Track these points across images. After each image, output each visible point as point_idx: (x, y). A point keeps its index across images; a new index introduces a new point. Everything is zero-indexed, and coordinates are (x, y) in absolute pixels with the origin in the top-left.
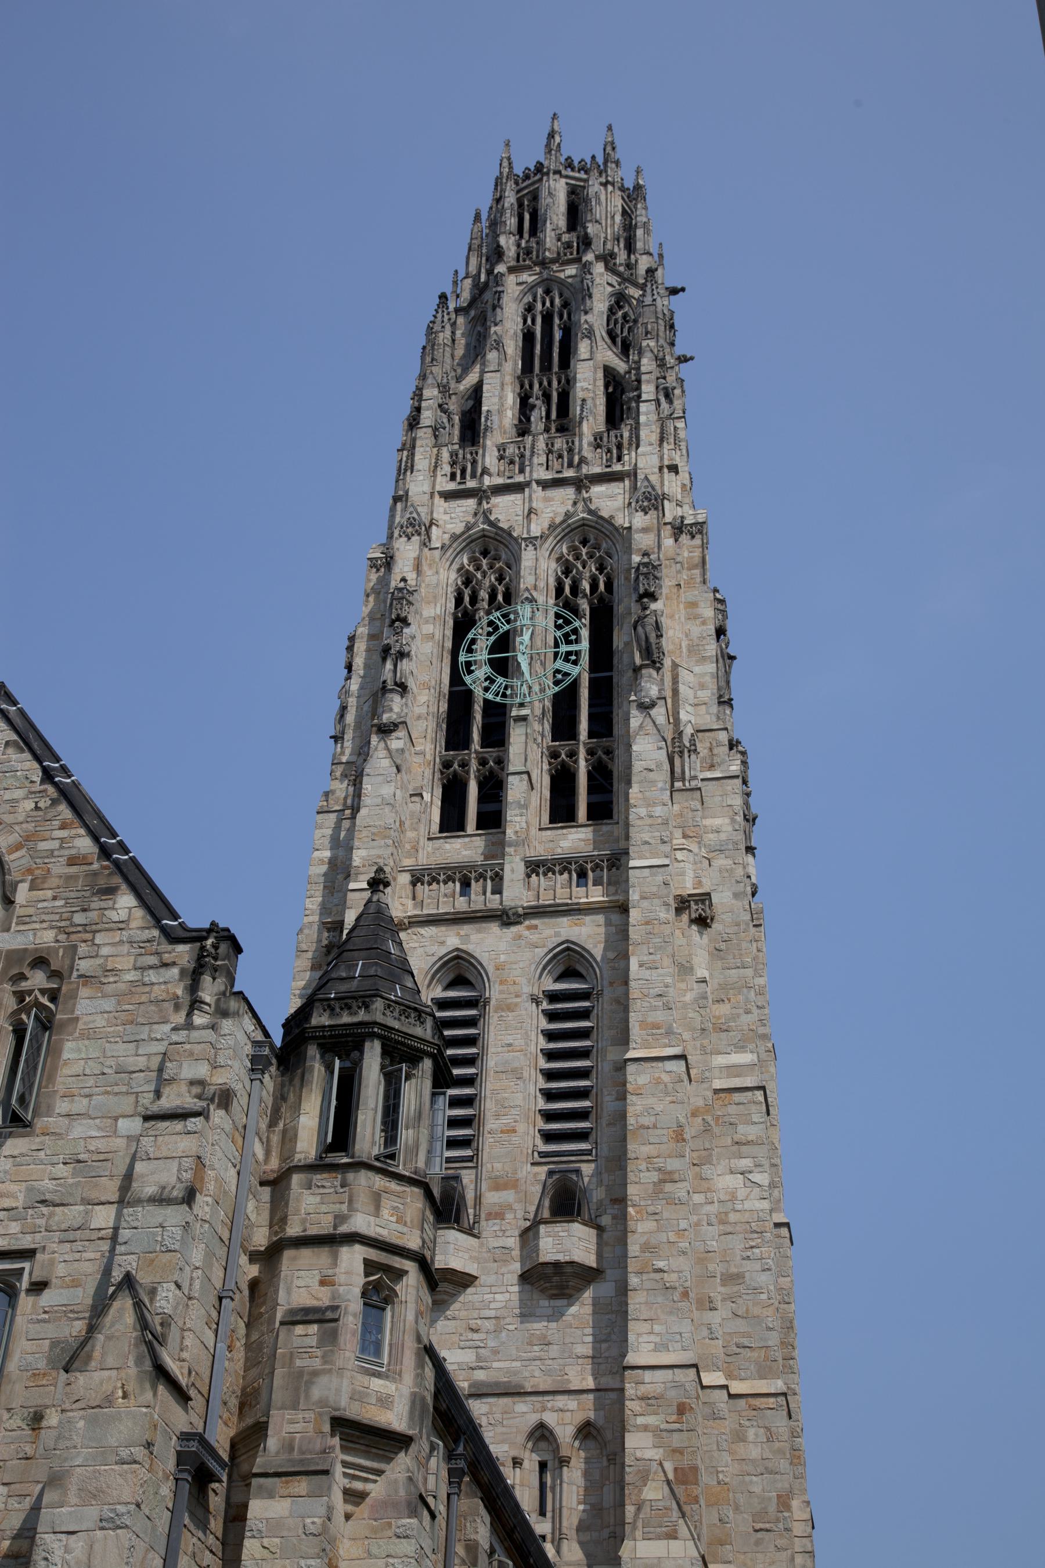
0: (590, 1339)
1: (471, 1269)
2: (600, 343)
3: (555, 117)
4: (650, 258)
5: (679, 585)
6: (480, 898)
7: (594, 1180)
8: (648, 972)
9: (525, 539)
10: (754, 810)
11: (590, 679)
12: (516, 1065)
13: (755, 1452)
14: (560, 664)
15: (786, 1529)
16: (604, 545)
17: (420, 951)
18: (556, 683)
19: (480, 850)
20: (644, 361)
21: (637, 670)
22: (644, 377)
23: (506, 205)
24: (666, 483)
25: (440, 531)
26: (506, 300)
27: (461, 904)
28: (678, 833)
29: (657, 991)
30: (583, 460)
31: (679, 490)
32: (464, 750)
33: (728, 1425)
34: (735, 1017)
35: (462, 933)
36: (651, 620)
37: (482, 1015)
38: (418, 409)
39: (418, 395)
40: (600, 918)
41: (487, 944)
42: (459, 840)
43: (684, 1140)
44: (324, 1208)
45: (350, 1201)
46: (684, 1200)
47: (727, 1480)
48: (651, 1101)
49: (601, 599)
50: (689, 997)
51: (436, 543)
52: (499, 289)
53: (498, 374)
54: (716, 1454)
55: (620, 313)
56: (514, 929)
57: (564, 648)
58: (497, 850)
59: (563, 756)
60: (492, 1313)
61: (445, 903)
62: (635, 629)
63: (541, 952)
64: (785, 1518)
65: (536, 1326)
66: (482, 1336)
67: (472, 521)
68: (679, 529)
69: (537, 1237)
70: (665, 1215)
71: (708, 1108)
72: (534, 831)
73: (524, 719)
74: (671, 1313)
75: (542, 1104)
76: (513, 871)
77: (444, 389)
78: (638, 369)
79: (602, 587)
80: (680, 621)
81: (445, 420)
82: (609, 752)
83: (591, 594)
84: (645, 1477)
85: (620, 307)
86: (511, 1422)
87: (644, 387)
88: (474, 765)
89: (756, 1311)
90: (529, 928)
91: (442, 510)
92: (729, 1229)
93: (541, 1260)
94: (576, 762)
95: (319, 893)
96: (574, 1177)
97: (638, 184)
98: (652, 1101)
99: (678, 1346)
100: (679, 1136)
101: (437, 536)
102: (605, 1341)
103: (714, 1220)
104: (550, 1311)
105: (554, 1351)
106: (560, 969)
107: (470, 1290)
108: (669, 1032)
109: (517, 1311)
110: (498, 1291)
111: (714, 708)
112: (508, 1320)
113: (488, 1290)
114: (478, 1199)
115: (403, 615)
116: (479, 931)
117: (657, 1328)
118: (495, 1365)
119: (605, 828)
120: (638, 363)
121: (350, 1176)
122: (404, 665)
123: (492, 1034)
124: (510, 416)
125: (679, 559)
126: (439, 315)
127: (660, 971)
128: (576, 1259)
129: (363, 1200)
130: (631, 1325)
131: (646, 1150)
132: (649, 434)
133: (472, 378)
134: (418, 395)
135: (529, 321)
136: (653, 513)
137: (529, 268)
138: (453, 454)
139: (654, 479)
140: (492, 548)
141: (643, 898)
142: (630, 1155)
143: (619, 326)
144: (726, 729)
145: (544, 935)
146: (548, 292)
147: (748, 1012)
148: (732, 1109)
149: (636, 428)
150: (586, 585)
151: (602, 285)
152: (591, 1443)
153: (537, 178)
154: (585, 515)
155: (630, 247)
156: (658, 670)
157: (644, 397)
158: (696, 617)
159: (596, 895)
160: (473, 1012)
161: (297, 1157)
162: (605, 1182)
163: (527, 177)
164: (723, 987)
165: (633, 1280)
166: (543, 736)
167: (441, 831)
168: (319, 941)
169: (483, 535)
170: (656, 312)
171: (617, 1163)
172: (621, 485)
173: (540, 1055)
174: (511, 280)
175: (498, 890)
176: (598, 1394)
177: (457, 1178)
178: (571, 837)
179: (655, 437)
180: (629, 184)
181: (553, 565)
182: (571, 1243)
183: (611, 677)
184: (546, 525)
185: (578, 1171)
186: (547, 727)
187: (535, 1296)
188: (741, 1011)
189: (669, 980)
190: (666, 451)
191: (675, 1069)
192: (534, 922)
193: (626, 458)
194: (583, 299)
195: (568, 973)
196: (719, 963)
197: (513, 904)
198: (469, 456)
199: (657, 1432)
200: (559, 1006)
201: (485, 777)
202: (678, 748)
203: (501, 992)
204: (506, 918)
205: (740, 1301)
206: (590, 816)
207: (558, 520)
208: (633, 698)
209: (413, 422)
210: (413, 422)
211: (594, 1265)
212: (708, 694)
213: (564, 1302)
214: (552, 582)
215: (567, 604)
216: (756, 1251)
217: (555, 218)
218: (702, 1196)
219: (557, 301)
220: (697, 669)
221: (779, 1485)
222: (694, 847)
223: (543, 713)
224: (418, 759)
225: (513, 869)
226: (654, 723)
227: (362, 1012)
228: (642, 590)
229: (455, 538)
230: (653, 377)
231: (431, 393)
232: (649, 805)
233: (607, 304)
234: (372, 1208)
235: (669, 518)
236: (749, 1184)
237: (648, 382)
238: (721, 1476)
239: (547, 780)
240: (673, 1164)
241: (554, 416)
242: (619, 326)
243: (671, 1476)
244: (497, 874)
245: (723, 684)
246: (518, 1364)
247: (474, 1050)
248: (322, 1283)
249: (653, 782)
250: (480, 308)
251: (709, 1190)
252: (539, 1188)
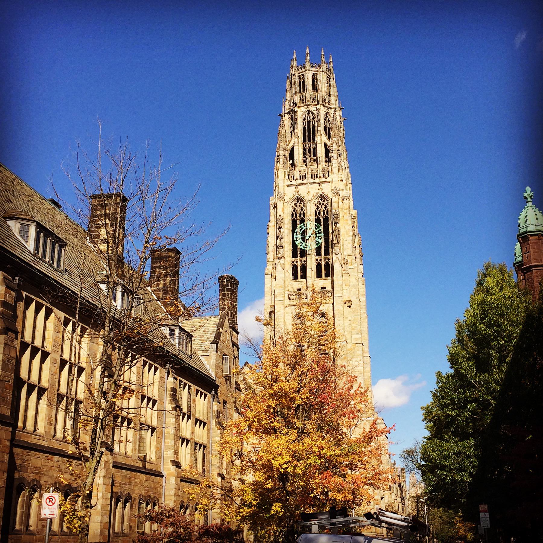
14: (317, 239)
18: (317, 244)
57: (318, 235)
101: (287, 198)
132: (336, 170)
146: (309, 114)
214: (314, 212)
215: (318, 221)
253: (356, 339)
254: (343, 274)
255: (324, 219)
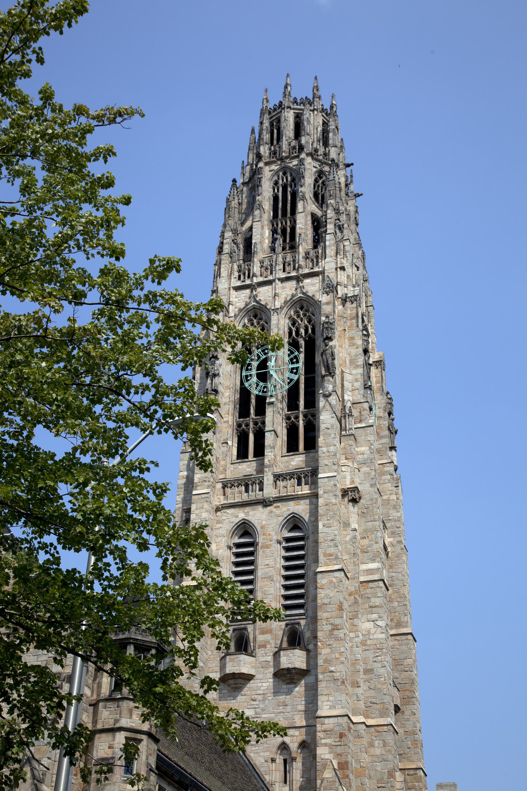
0: (303, 703)
1: (252, 672)
2: (309, 201)
3: (288, 75)
4: (336, 149)
5: (345, 330)
6: (255, 494)
7: (306, 627)
8: (327, 529)
9: (273, 310)
10: (396, 426)
11: (305, 378)
12: (271, 574)
13: (378, 752)
15: (391, 786)
16: (311, 310)
17: (227, 520)
19: (255, 468)
20: (329, 211)
21: (323, 377)
22: (328, 221)
23: (264, 128)
24: (339, 276)
25: (234, 307)
26: (263, 180)
27: (245, 497)
28: (343, 457)
29: (331, 538)
30: (300, 267)
31: (346, 279)
32: (246, 417)
33: (365, 742)
34: (370, 546)
35: (246, 511)
36: (329, 352)
37: (255, 550)
38: (222, 243)
39: (222, 236)
40: (307, 501)
41: (257, 516)
42: (245, 464)
43: (343, 610)
44: (111, 717)
45: (120, 713)
46: (343, 638)
47: (364, 765)
48: (328, 591)
49: (310, 337)
50: (348, 538)
51: (232, 314)
52: (260, 176)
53: (260, 223)
54: (359, 754)
55: (321, 181)
56: (269, 508)
58: (260, 470)
59: (293, 419)
60: (261, 692)
61: (238, 497)
62: (322, 356)
63: (281, 519)
64: (391, 782)
65: (281, 697)
66: (257, 703)
67: (248, 301)
68: (344, 300)
69: (279, 657)
70: (334, 645)
71: (356, 592)
72: (279, 458)
73: (272, 403)
74: (337, 691)
75: (283, 592)
76: (268, 480)
77: (235, 232)
78: (326, 215)
79: (310, 331)
80: (344, 348)
81: (235, 248)
82: (314, 416)
83: (305, 335)
84: (325, 766)
85: (321, 178)
86: (270, 742)
87: (328, 226)
88: (251, 425)
89: (379, 686)
90: (276, 507)
91: (234, 296)
92: (367, 648)
93: (281, 668)
94: (298, 421)
95: (182, 493)
96: (297, 626)
97: (333, 104)
98: (328, 591)
99: (340, 706)
100: (341, 608)
102: (311, 703)
103: (359, 645)
104: (287, 690)
105: (289, 708)
106: (291, 526)
107: (252, 682)
108: (337, 558)
109: (272, 691)
110: (264, 682)
111: (362, 392)
112: (269, 695)
113: (259, 681)
114: (255, 638)
115: (215, 355)
116: (253, 510)
117: (331, 698)
118: (263, 716)
119: (311, 455)
120: (326, 212)
121: (121, 703)
122: (216, 380)
123: (260, 560)
124: (267, 242)
125: (345, 316)
126: (232, 191)
127: (332, 528)
128: (297, 666)
129: (125, 712)
130: (319, 697)
131: (325, 615)
132: (330, 251)
133: (248, 224)
134: (222, 236)
135: (276, 191)
136: (331, 294)
137: (275, 162)
138: (239, 266)
139: (332, 276)
140: (258, 314)
141: (325, 493)
142: (319, 618)
143: (320, 188)
144: (367, 402)
145: (283, 510)
146: (285, 174)
147: (377, 543)
148: (369, 591)
149: (325, 248)
150: (302, 331)
151: (310, 168)
152: (306, 750)
153: (279, 110)
154: (301, 295)
155: (326, 144)
156: (333, 377)
157: (328, 231)
158: (354, 345)
159: (306, 490)
160: (251, 549)
161: (102, 695)
162: (311, 629)
163: (275, 109)
164: (365, 531)
165: (320, 677)
166: (283, 409)
167: (237, 459)
168: (182, 517)
169: (254, 308)
170: (335, 184)
171: (314, 620)
172: (318, 278)
173: (282, 568)
174: (267, 168)
175: (261, 489)
176: (308, 728)
177: (245, 629)
178: (296, 459)
179: (333, 253)
180: (327, 106)
181: (287, 321)
182: (295, 659)
183: (314, 377)
184: (283, 301)
185: (299, 624)
186: (285, 404)
187: (280, 683)
188: (373, 542)
189: (336, 532)
190: (339, 259)
191: (338, 575)
192: (278, 504)
193: (320, 264)
194: (300, 179)
195: (295, 527)
196: (364, 519)
197: (268, 496)
198: (246, 267)
199: (330, 746)
200: (290, 544)
201: (257, 431)
202: (343, 416)
203: (264, 539)
204: (265, 503)
205: (372, 682)
206: (305, 449)
207: (288, 298)
208: (321, 392)
209: (220, 250)
210: (220, 250)
211: (305, 668)
212: (359, 385)
213: (292, 686)
216: (379, 658)
217: (287, 133)
218: (354, 634)
219: (289, 178)
220: (354, 372)
221: (389, 767)
222: (350, 464)
223: (283, 397)
224: (225, 425)
225: (268, 479)
226: (330, 404)
227: (127, 633)
228: (325, 336)
229: (240, 310)
230: (333, 220)
231: (228, 234)
232: (328, 446)
233: (314, 178)
234: (129, 716)
235: (340, 295)
236: (376, 626)
237: (330, 223)
238: (362, 764)
239: (285, 431)
240: (337, 621)
241: (288, 241)
242: (320, 188)
243: (336, 767)
244: (261, 481)
245: (366, 378)
246: (273, 715)
247: (252, 567)
248: (109, 748)
249: (329, 435)
250: (253, 182)
251: (357, 631)
252: (282, 632)
253: (370, 572)
254: (341, 436)
255: (306, 342)
